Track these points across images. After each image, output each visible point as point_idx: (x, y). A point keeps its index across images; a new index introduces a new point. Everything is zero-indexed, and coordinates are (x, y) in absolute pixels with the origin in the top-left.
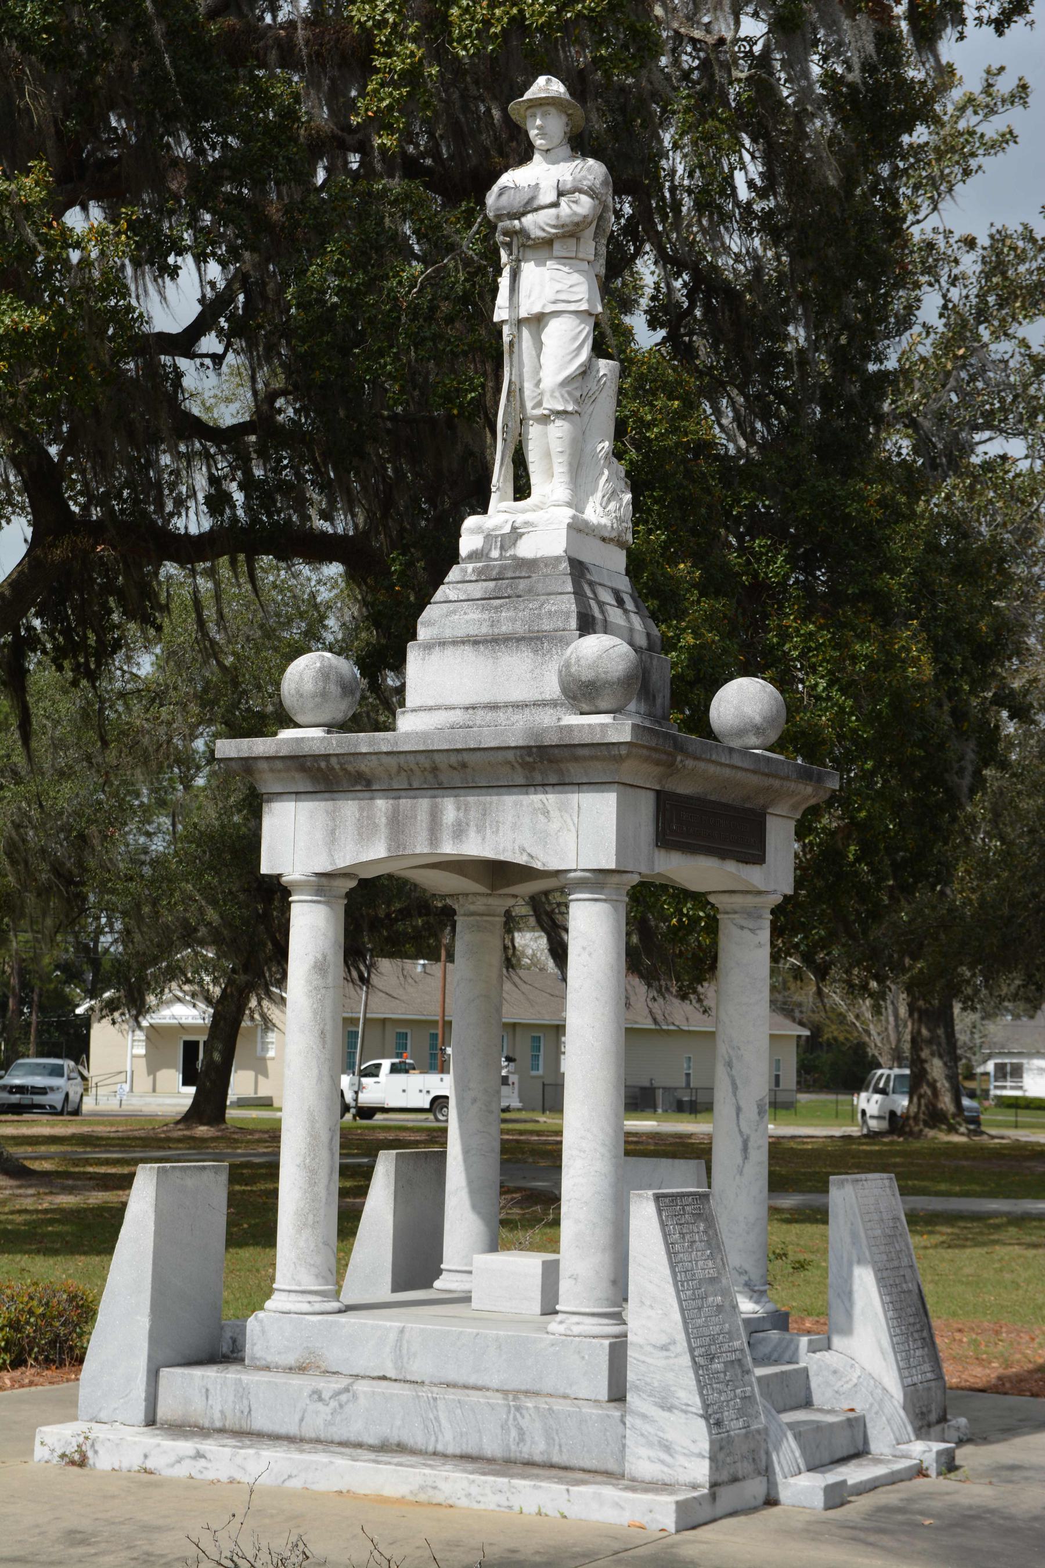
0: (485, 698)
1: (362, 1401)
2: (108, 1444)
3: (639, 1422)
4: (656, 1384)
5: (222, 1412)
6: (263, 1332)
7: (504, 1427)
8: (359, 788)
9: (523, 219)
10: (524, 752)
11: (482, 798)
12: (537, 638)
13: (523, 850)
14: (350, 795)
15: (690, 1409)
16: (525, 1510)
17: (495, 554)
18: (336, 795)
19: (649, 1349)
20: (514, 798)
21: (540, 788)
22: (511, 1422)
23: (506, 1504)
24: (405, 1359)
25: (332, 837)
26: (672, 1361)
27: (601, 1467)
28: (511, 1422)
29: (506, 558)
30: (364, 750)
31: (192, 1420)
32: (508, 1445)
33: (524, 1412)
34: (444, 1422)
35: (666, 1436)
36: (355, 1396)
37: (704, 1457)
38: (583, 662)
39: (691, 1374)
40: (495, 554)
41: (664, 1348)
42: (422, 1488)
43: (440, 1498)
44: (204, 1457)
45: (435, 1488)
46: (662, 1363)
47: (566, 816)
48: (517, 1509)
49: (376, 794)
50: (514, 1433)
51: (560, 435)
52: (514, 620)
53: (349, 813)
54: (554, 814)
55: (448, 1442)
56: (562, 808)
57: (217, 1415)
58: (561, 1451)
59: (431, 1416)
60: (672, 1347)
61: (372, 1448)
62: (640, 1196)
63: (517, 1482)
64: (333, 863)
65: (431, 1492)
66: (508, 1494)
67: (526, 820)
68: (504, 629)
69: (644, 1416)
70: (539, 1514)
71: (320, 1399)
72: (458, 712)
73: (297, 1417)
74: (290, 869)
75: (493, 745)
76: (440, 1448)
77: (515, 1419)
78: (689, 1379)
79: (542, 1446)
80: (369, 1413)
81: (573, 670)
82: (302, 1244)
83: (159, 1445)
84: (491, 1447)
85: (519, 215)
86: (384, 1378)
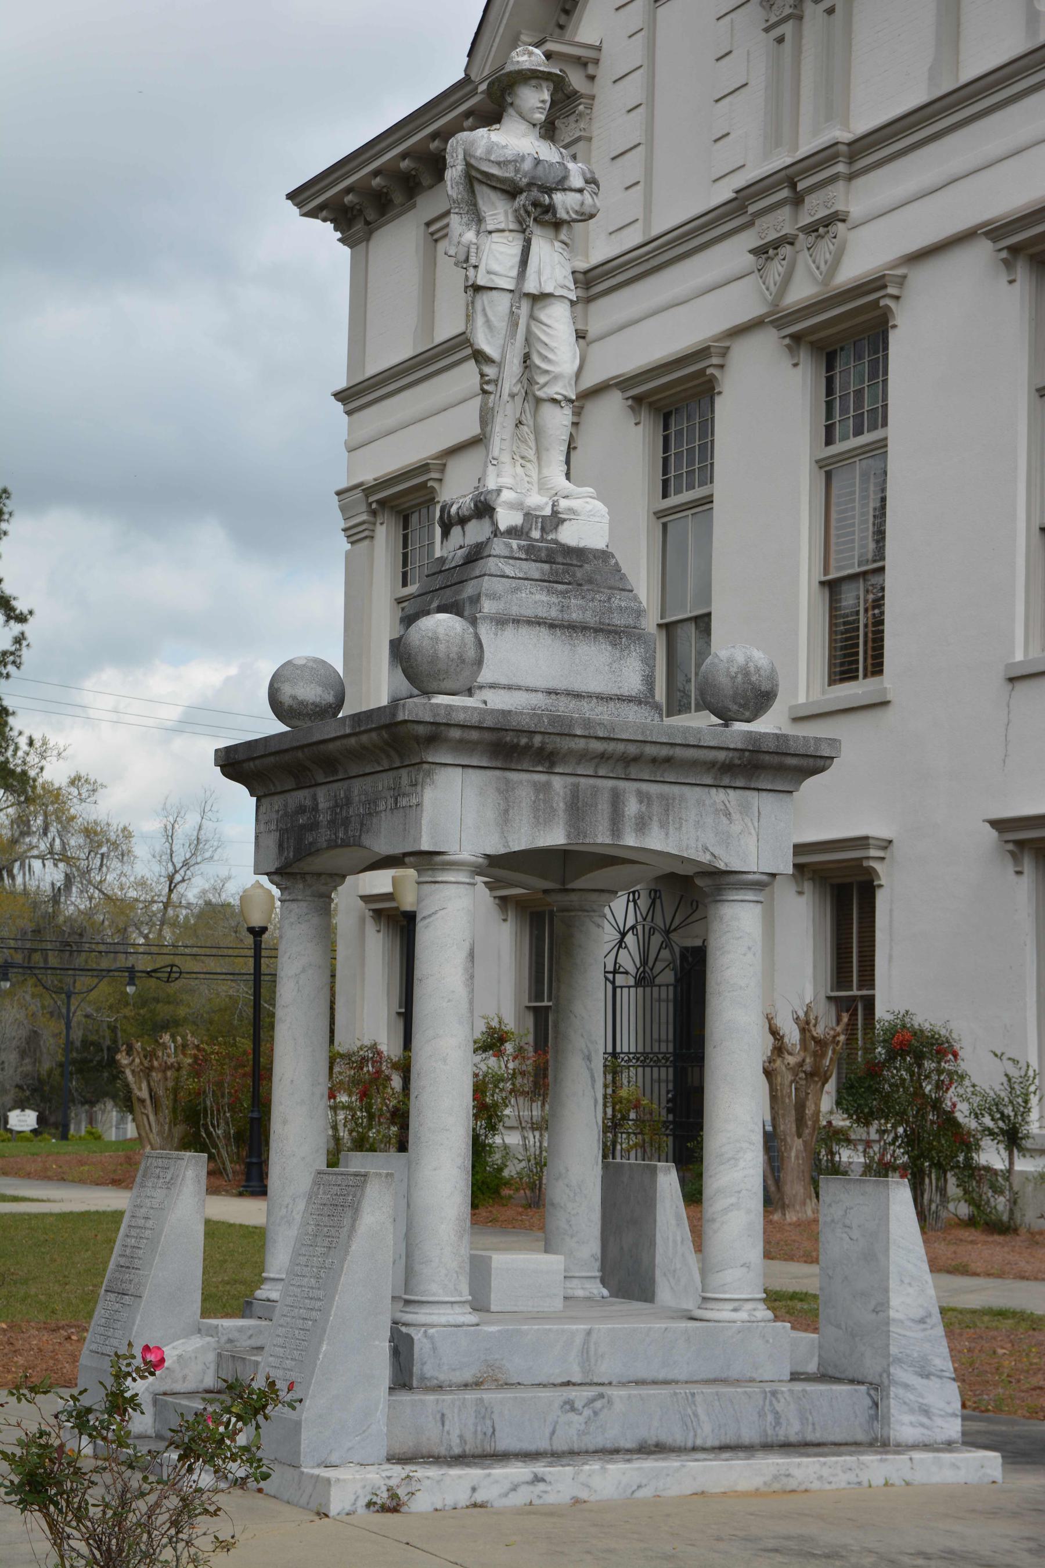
0: (561, 684)
1: (618, 1406)
2: (427, 1482)
3: (901, 1391)
4: (916, 1355)
5: (461, 1437)
6: (434, 1349)
7: (761, 1414)
8: (540, 769)
12: (616, 632)
13: (706, 849)
16: (873, 1483)
17: (536, 534)
19: (909, 1323)
22: (767, 1407)
23: (856, 1480)
24: (593, 1361)
25: (505, 817)
26: (929, 1332)
27: (850, 1439)
28: (767, 1407)
29: (547, 541)
31: (425, 1451)
32: (765, 1431)
33: (779, 1396)
34: (703, 1417)
35: (925, 1401)
36: (610, 1402)
37: (956, 1416)
38: (762, 672)
39: (944, 1342)
40: (536, 534)
41: (922, 1321)
42: (776, 1478)
43: (792, 1484)
44: (543, 1480)
45: (788, 1475)
46: (921, 1335)
47: (747, 820)
48: (865, 1484)
50: (770, 1418)
52: (584, 609)
53: (524, 794)
55: (707, 1435)
57: (455, 1441)
58: (814, 1429)
59: (689, 1411)
60: (928, 1320)
61: (713, 1449)
63: (865, 1458)
64: (506, 844)
65: (784, 1480)
67: (709, 820)
68: (574, 616)
69: (906, 1386)
70: (886, 1484)
71: (573, 1409)
72: (540, 695)
73: (547, 1432)
76: (699, 1442)
77: (771, 1404)
80: (624, 1417)
81: (754, 679)
83: (489, 1475)
84: (749, 1435)
85: (549, 191)
86: (568, 1384)
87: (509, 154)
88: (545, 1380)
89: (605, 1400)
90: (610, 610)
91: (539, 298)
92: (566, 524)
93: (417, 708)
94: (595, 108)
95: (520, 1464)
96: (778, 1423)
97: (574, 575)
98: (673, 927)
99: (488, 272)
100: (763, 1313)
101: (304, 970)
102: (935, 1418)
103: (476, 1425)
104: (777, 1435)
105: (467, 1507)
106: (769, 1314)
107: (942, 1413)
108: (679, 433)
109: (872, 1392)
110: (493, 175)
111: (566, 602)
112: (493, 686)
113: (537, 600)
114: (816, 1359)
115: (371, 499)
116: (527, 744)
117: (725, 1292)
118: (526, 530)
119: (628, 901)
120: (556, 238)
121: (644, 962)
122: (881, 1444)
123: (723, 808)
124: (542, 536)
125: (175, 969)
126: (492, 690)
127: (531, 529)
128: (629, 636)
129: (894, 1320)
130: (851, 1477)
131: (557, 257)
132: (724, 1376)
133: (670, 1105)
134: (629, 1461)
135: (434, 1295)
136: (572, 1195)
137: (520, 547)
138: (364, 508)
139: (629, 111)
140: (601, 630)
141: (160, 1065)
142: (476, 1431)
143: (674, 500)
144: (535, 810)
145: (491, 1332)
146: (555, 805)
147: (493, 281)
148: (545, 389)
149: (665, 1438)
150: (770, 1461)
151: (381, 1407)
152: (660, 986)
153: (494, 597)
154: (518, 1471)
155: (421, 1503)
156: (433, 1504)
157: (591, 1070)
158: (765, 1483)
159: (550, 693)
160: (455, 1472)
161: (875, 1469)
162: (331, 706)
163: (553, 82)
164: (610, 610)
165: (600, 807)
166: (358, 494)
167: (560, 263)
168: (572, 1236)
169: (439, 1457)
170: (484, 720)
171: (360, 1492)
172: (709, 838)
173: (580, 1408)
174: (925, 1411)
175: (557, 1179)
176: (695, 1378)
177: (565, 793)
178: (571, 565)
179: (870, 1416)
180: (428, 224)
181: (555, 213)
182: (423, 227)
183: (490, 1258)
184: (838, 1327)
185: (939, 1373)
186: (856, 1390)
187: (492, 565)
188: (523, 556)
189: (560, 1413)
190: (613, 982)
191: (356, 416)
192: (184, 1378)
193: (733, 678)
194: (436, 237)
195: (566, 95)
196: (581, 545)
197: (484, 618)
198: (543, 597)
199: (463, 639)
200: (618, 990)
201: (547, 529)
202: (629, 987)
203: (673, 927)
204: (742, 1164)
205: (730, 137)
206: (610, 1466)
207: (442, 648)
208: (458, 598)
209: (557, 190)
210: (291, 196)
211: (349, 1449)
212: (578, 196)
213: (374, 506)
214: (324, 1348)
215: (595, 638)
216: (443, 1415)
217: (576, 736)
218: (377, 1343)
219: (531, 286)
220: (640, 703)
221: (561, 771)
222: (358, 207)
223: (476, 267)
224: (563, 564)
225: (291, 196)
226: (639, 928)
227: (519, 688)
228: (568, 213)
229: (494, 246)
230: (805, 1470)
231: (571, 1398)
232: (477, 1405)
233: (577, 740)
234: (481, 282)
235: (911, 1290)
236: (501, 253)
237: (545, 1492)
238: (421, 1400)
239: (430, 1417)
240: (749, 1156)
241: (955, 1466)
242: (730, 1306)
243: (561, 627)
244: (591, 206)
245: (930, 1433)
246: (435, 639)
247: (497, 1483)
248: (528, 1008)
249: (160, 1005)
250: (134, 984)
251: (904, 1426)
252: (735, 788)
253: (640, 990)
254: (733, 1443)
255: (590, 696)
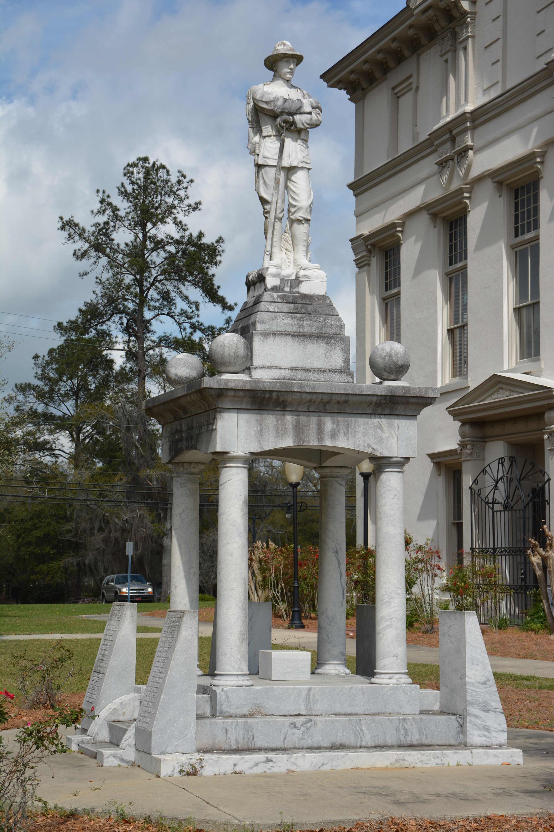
1: (320, 725)
2: (210, 761)
3: (473, 719)
5: (236, 740)
6: (227, 697)
7: (397, 730)
8: (278, 409)
9: (295, 117)
10: (382, 398)
11: (346, 419)
12: (328, 337)
13: (369, 446)
14: (271, 412)
15: (497, 710)
16: (451, 764)
17: (287, 289)
18: (262, 412)
20: (364, 419)
21: (377, 416)
23: (441, 762)
24: (312, 704)
25: (260, 433)
26: (488, 689)
29: (293, 292)
30: (296, 390)
32: (399, 738)
34: (365, 731)
35: (486, 724)
36: (315, 723)
38: (399, 355)
39: (497, 694)
40: (287, 289)
41: (484, 683)
42: (397, 761)
43: (406, 764)
44: (271, 761)
45: (404, 760)
47: (392, 431)
48: (447, 765)
49: (286, 413)
50: (402, 732)
51: (306, 231)
53: (270, 422)
54: (386, 429)
55: (368, 740)
56: (390, 426)
57: (233, 742)
58: (427, 738)
59: (358, 729)
60: (488, 683)
62: (470, 613)
65: (402, 762)
66: (442, 758)
67: (371, 431)
68: (306, 330)
69: (476, 716)
70: (458, 765)
71: (295, 727)
72: (287, 371)
74: (235, 449)
75: (368, 393)
76: (363, 744)
77: (403, 725)
78: (496, 697)
79: (417, 737)
81: (394, 359)
82: (243, 649)
83: (243, 758)
85: (292, 114)
86: (299, 715)
87: (271, 97)
88: (286, 713)
89: (313, 723)
90: (326, 326)
91: (290, 170)
92: (303, 283)
93: (209, 382)
94: (476, 19)
95: (263, 753)
96: (407, 734)
97: (307, 309)
98: (522, 477)
99: (264, 157)
100: (406, 679)
101: (184, 511)
102: (492, 733)
103: (244, 734)
104: (406, 741)
105: (232, 773)
106: (410, 680)
107: (496, 730)
108: (523, 201)
109: (459, 719)
110: (264, 108)
111: (301, 323)
112: (262, 367)
113: (286, 323)
114: (438, 703)
115: (368, 243)
116: (269, 397)
117: (385, 669)
118: (282, 287)
119: (499, 463)
120: (299, 138)
121: (508, 497)
122: (464, 745)
123: (378, 425)
124: (290, 290)
125: (303, 504)
126: (261, 369)
127: (284, 287)
128: (335, 338)
129: (468, 683)
130: (439, 761)
131: (299, 147)
132: (383, 711)
133: (523, 576)
134: (320, 752)
135: (228, 671)
136: (329, 622)
137: (278, 296)
138: (364, 248)
139: (494, 20)
140: (320, 337)
141: (256, 558)
142: (244, 737)
143: (521, 238)
144: (277, 429)
145: (257, 689)
146: (287, 427)
147: (266, 161)
148: (295, 215)
149: (345, 741)
150: (394, 753)
151: (192, 725)
152: (516, 511)
153: (262, 322)
154: (260, 757)
155: (208, 771)
156: (213, 772)
157: (338, 559)
158: (391, 764)
159: (292, 369)
160: (225, 757)
161: (453, 758)
162: (195, 378)
163: (297, 58)
164: (326, 326)
165: (311, 427)
166: (361, 241)
167: (301, 150)
168: (329, 643)
169: (225, 750)
170: (245, 386)
171: (176, 766)
172: (371, 441)
173: (299, 726)
174: (487, 729)
175: (322, 614)
176: (367, 713)
177: (292, 420)
178: (306, 304)
179: (458, 731)
180: (393, 89)
181: (296, 126)
182: (390, 90)
183: (270, 654)
184: (447, 687)
185: (494, 710)
186: (450, 719)
187: (263, 306)
188: (280, 301)
189: (288, 729)
190: (492, 509)
191: (360, 197)
192: (124, 713)
193: (384, 359)
194: (398, 95)
195: (460, 13)
196: (312, 293)
197: (257, 333)
198: (289, 321)
199: (237, 345)
200: (495, 513)
201: (293, 286)
202: (500, 511)
203: (522, 477)
204: (393, 604)
205: (545, 33)
206: (308, 755)
207: (226, 350)
208: (248, 323)
209: (298, 114)
210: (322, 77)
211: (176, 745)
212: (309, 116)
213: (369, 247)
214: (163, 696)
215: (317, 340)
216: (227, 730)
217: (294, 392)
218: (190, 694)
219: (285, 163)
220: (341, 372)
221: (290, 409)
222: (357, 81)
223: (258, 155)
224: (301, 304)
225: (322, 77)
226: (505, 478)
227: (276, 368)
228: (303, 125)
229: (267, 144)
230: (413, 758)
231: (294, 721)
232: (244, 725)
233: (295, 394)
234: (260, 162)
235: (478, 668)
236: (270, 147)
237: (273, 767)
238: (215, 722)
239: (217, 731)
240: (397, 600)
241: (496, 756)
242: (388, 676)
243: (298, 336)
244: (316, 121)
245: (489, 740)
246: (223, 346)
247: (247, 763)
248: (453, 523)
249: (314, 524)
250: (290, 513)
251: (475, 736)
252: (385, 415)
253: (506, 512)
254: (382, 745)
255: (314, 370)
